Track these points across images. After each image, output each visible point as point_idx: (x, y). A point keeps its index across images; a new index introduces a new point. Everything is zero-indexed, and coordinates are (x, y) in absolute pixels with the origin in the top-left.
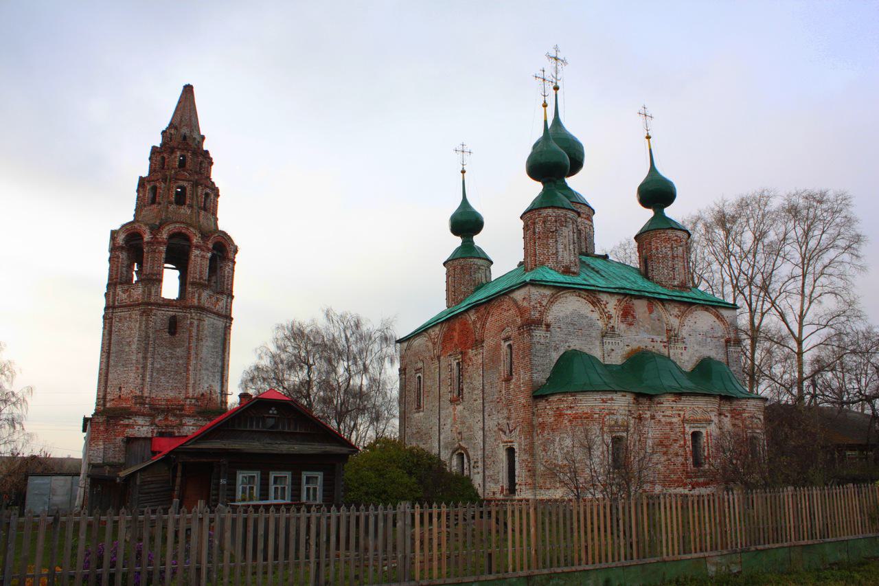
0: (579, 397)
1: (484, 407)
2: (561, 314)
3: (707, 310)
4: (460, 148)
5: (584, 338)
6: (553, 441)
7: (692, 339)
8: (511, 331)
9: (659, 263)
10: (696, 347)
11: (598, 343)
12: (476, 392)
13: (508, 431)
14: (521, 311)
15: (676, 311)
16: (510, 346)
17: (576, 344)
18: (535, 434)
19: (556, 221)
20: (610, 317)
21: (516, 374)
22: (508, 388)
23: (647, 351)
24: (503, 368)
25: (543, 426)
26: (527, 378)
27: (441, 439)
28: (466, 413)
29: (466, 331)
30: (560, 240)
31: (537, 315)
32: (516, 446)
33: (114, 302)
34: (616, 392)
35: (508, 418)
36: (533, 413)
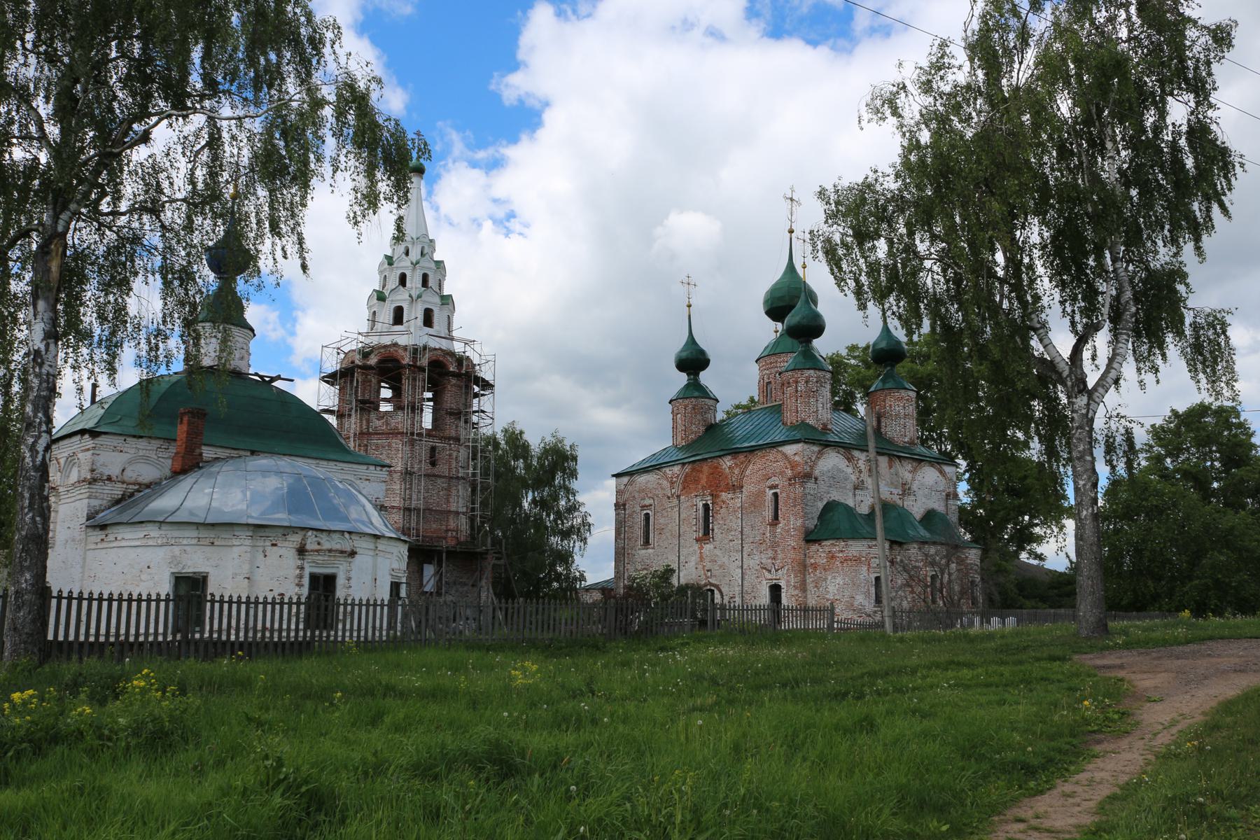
0: (850, 543)
2: (825, 469)
3: (932, 466)
4: (686, 280)
6: (825, 580)
10: (924, 500)
11: (851, 494)
12: (733, 533)
15: (909, 467)
16: (776, 495)
17: (835, 496)
20: (860, 472)
22: (773, 533)
24: (768, 514)
25: (815, 566)
28: (717, 552)
32: (783, 584)
33: (368, 428)
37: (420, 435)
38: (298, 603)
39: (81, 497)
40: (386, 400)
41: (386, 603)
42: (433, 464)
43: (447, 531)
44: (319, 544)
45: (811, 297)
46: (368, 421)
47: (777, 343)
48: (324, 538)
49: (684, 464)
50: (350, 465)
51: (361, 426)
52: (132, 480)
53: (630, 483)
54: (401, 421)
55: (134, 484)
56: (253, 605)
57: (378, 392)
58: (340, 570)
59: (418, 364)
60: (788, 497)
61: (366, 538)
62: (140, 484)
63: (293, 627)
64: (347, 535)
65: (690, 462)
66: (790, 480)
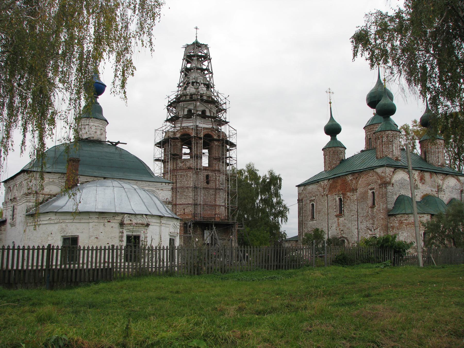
1: (358, 219)
2: (397, 179)
3: (453, 177)
4: (328, 91)
5: (406, 190)
7: (447, 190)
8: (376, 186)
9: (432, 154)
10: (449, 194)
12: (353, 212)
13: (373, 230)
14: (381, 178)
16: (373, 193)
17: (403, 192)
18: (389, 231)
19: (392, 137)
21: (377, 205)
22: (372, 211)
23: (430, 195)
24: (370, 202)
26: (384, 207)
27: (329, 233)
28: (346, 221)
29: (345, 184)
30: (394, 145)
31: (389, 180)
34: (425, 213)
35: (373, 224)
36: (388, 222)
37: (200, 169)
38: (121, 249)
39: (23, 202)
40: (185, 154)
41: (60, 248)
42: (208, 183)
43: (215, 214)
44: (131, 221)
45: (391, 97)
46: (176, 164)
47: (373, 119)
48: (133, 218)
49: (329, 179)
50: (153, 183)
51: (173, 166)
52: (47, 193)
53: (304, 189)
54: (192, 164)
55: (48, 195)
56: (99, 251)
57: (181, 150)
58: (141, 233)
59: (199, 136)
60: (379, 193)
61: (155, 217)
62: (51, 195)
63: (119, 261)
64: (144, 216)
65: (332, 178)
66: (380, 185)
